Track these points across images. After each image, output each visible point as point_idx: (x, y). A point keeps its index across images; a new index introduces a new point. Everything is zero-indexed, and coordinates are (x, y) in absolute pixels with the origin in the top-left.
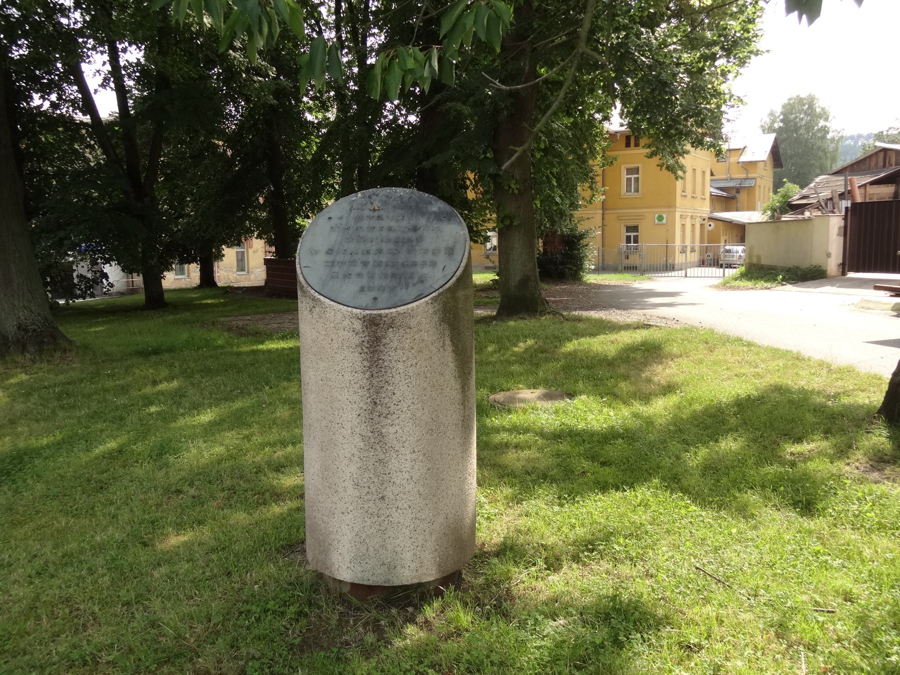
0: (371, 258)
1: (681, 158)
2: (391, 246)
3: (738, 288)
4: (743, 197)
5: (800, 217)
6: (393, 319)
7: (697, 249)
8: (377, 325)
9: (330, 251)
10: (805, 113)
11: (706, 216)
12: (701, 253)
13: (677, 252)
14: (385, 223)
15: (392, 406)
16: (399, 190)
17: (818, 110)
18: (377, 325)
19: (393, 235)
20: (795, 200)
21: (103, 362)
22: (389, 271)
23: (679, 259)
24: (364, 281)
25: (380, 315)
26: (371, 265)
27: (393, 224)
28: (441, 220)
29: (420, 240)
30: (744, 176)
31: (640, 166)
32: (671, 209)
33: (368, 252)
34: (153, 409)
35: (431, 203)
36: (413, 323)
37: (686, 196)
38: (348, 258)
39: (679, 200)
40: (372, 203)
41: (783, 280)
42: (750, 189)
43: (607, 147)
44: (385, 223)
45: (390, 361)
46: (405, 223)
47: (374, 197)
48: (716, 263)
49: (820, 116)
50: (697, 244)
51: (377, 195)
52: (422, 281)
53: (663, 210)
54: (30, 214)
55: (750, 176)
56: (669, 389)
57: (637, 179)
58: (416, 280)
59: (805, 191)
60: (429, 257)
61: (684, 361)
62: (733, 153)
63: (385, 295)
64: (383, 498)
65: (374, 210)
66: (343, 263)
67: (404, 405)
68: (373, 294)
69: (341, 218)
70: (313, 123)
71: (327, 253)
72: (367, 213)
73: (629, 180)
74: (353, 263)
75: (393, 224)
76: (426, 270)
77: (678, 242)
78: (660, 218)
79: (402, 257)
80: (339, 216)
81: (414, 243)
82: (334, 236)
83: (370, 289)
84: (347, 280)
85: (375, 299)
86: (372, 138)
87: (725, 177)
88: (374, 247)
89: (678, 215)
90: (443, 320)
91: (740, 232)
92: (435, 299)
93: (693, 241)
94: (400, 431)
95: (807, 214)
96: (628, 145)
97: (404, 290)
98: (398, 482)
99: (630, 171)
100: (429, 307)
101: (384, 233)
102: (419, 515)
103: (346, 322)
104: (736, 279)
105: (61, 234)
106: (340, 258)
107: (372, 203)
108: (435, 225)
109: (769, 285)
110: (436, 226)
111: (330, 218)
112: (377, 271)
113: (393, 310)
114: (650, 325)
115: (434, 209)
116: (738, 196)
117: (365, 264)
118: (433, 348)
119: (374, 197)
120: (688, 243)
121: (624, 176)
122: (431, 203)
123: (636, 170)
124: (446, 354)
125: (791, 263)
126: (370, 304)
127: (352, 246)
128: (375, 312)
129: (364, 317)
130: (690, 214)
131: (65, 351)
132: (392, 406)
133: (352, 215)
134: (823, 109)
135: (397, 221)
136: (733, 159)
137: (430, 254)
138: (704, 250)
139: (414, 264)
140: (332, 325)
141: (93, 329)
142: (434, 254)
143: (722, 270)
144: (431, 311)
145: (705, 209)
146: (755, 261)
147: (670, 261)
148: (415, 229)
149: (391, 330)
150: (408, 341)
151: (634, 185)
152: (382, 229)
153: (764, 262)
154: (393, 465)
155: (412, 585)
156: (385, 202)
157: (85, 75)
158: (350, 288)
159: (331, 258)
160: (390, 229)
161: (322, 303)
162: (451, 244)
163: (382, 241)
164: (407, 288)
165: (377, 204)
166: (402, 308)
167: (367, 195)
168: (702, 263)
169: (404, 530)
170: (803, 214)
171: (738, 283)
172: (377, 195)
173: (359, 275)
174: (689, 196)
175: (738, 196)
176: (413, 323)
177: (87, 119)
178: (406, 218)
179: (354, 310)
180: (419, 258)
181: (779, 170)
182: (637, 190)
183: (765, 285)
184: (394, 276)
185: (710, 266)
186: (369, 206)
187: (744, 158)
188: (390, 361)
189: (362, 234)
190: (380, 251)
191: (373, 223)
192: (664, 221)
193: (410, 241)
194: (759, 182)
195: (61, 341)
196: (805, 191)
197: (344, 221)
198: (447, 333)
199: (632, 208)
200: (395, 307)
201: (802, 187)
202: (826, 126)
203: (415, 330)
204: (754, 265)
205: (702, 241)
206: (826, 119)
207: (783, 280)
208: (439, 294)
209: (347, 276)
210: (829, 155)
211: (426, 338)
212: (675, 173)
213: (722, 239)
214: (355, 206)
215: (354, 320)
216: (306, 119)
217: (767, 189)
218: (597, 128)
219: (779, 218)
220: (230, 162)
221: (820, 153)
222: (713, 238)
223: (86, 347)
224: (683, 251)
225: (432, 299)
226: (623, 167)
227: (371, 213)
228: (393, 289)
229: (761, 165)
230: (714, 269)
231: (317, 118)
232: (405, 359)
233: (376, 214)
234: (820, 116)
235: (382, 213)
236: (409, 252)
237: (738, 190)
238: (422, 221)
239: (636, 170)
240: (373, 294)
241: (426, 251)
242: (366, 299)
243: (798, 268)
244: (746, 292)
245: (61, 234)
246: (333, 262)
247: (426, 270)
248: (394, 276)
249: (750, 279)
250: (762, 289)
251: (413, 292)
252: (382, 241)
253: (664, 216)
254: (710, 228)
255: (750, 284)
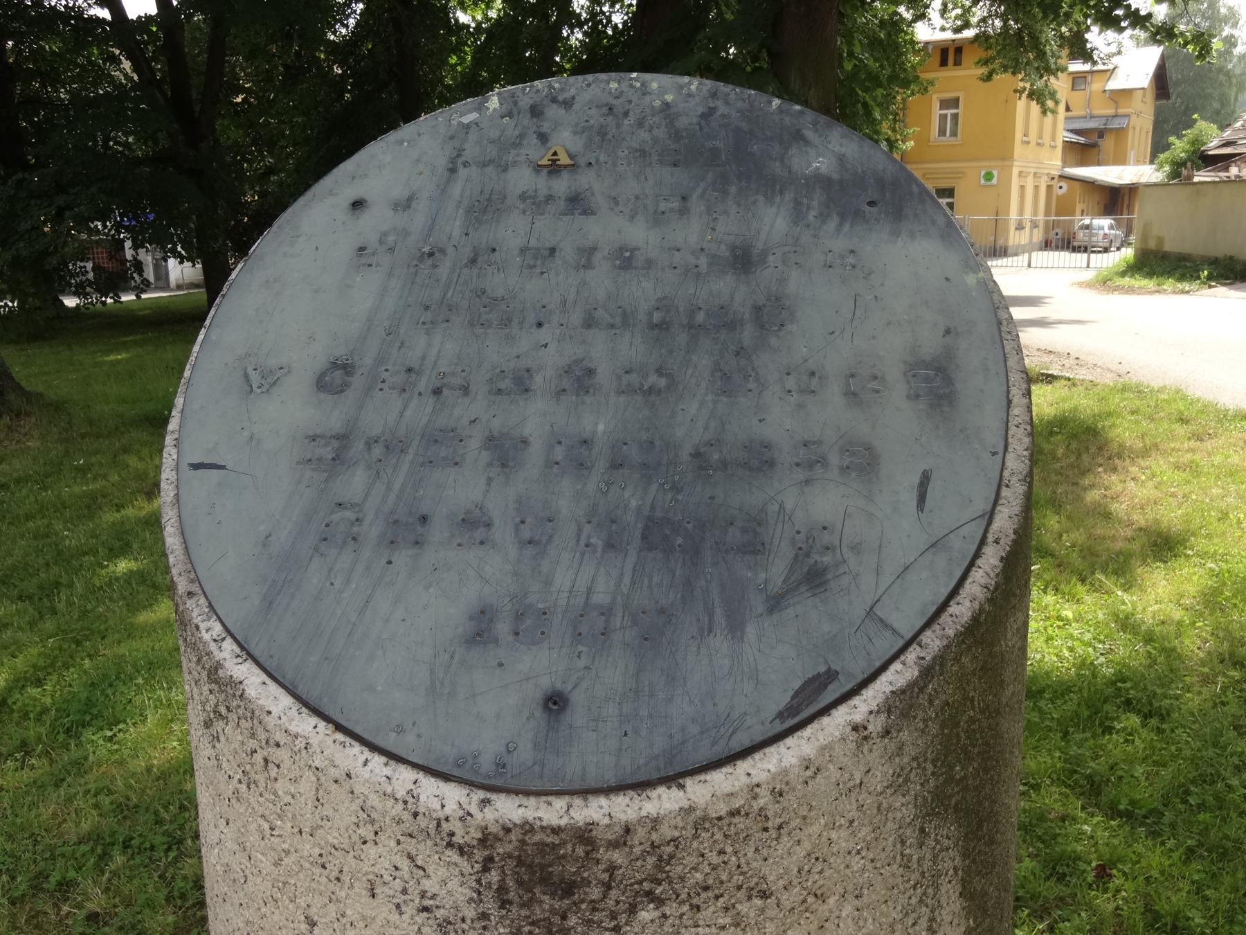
0: (535, 418)
1: (1052, 79)
2: (632, 348)
3: (1130, 290)
4: (1108, 144)
5: (1222, 174)
6: (663, 855)
7: (1041, 225)
8: (568, 888)
9: (335, 377)
10: (1203, 16)
11: (1056, 173)
12: (1046, 231)
13: (1012, 228)
14: (606, 229)
16: (655, 81)
17: (1223, 11)
18: (568, 888)
19: (642, 292)
20: (1213, 146)
21: (83, 436)
22: (633, 499)
23: (1015, 238)
24: (488, 573)
25: (584, 835)
26: (535, 455)
27: (638, 234)
28: (857, 215)
29: (771, 315)
30: (1111, 112)
31: (961, 95)
32: (1007, 163)
33: (522, 384)
34: (123, 566)
35: (798, 137)
36: (780, 862)
37: (1028, 143)
38: (419, 412)
39: (1018, 149)
40: (543, 138)
41: (1210, 278)
42: (1120, 132)
43: (920, 64)
44: (606, 229)
46: (689, 232)
47: (553, 112)
48: (1068, 243)
49: (1225, 20)
50: (1041, 217)
51: (568, 104)
52: (813, 578)
53: (993, 164)
55: (1121, 111)
56: (1164, 545)
57: (955, 117)
58: (777, 570)
59: (1228, 134)
60: (830, 415)
61: (1158, 464)
62: (1096, 76)
63: (614, 671)
65: (554, 168)
66: (393, 446)
68: (542, 665)
69: (405, 204)
70: (468, 26)
71: (322, 384)
72: (522, 179)
73: (943, 118)
74: (440, 445)
75: (638, 234)
76: (826, 502)
77: (1013, 216)
78: (989, 176)
79: (692, 419)
80: (399, 193)
81: (747, 334)
82: (368, 293)
83: (529, 622)
84: (403, 557)
85: (555, 703)
86: (557, 52)
87: (1082, 113)
88: (550, 354)
89: (1015, 171)
90: (935, 806)
91: (1114, 200)
92: (901, 706)
93: (1035, 213)
95: (1234, 170)
96: (944, 63)
97: (720, 642)
99: (945, 104)
100: (875, 755)
101: (601, 280)
103: (382, 856)
104: (1123, 274)
105: (61, 201)
106: (381, 413)
107: (543, 138)
108: (835, 239)
109: (1186, 286)
110: (839, 244)
111: (358, 205)
112: (567, 500)
113: (665, 801)
114: (1052, 376)
115: (820, 163)
116: (1100, 142)
117: (504, 451)
119: (553, 112)
120: (1028, 216)
121: (937, 112)
122: (798, 137)
123: (955, 103)
125: (1221, 249)
126: (525, 753)
127: (443, 349)
128: (552, 812)
129: (486, 840)
130: (1033, 170)
131: (18, 415)
133: (456, 190)
134: (1230, 9)
135: (658, 219)
136: (1096, 86)
137: (834, 394)
138: (1049, 226)
139: (759, 460)
140: (308, 848)
141: (112, 357)
142: (852, 396)
143: (1085, 255)
144: (880, 776)
145: (1054, 162)
146: (1152, 245)
147: (1001, 242)
148: (743, 260)
149: (647, 914)
151: (951, 127)
152: (587, 256)
153: (1168, 247)
156: (602, 132)
158: (407, 618)
159: (334, 416)
160: (625, 259)
161: (254, 715)
162: (930, 344)
163: (589, 323)
164: (736, 628)
165: (565, 142)
166: (721, 780)
167: (525, 102)
168: (1047, 245)
170: (1226, 169)
171: (1127, 281)
172: (568, 104)
173: (473, 524)
174: (1033, 143)
175: (1100, 142)
176: (780, 862)
177: (105, 14)
178: (697, 206)
179: (430, 789)
180: (779, 421)
181: (1164, 102)
182: (954, 134)
183: (1180, 286)
184: (657, 534)
185: (1057, 248)
186: (532, 150)
187: (1113, 85)
189: (496, 283)
190: (580, 379)
191: (553, 229)
192: (994, 181)
193: (725, 321)
194: (1134, 120)
195: (12, 397)
196: (1228, 134)
197: (418, 220)
198: (951, 861)
199: (948, 161)
200: (673, 779)
201: (1222, 128)
202: (1232, 36)
204: (1152, 252)
205: (1047, 213)
206: (1235, 25)
207: (1210, 278)
208: (927, 672)
209: (408, 529)
210: (1234, 81)
212: (1043, 105)
213: (1078, 211)
214: (471, 150)
215: (424, 851)
216: (457, 20)
217: (1144, 132)
218: (906, 33)
219: (1190, 177)
220: (338, 85)
221: (1222, 78)
222: (1063, 207)
223: (57, 407)
224: (1020, 227)
225: (887, 708)
226: (935, 97)
227: (542, 184)
228: (653, 634)
229: (1139, 94)
230: (1062, 253)
231: (474, 18)
233: (562, 185)
234: (1225, 20)
235: (585, 179)
236: (727, 382)
237: (1101, 134)
238: (772, 222)
239: (955, 103)
240: (542, 665)
241: (810, 382)
242: (495, 714)
243: (1231, 258)
244: (1126, 297)
245: (61, 201)
246: (343, 438)
247: (826, 502)
248: (657, 534)
249: (1150, 275)
250: (1174, 292)
251: (773, 658)
252: (589, 323)
253: (995, 173)
254: (1061, 192)
255: (1150, 284)
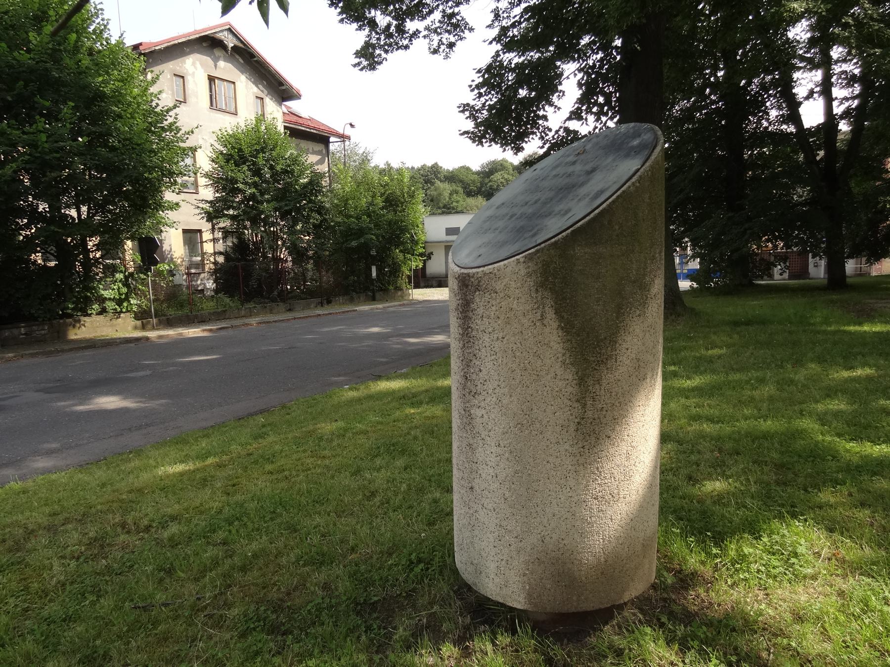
15: (480, 386)
45: (477, 330)
54: (387, 200)
64: (472, 488)
67: (490, 386)
90: (541, 285)
92: (530, 258)
94: (486, 416)
98: (484, 475)
100: (521, 266)
102: (504, 523)
118: (525, 321)
124: (547, 330)
132: (480, 386)
144: (523, 272)
150: (494, 308)
154: (480, 454)
155: (600, 610)
157: (802, 117)
169: (488, 535)
176: (499, 286)
188: (477, 330)
198: (549, 302)
203: (502, 295)
208: (538, 251)
211: (515, 306)
225: (525, 257)
232: (490, 330)
